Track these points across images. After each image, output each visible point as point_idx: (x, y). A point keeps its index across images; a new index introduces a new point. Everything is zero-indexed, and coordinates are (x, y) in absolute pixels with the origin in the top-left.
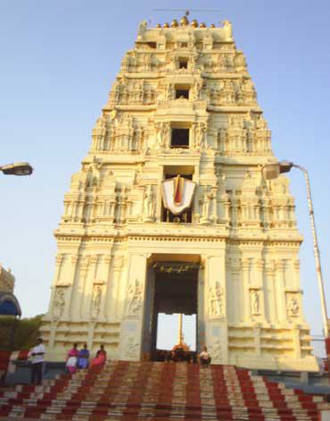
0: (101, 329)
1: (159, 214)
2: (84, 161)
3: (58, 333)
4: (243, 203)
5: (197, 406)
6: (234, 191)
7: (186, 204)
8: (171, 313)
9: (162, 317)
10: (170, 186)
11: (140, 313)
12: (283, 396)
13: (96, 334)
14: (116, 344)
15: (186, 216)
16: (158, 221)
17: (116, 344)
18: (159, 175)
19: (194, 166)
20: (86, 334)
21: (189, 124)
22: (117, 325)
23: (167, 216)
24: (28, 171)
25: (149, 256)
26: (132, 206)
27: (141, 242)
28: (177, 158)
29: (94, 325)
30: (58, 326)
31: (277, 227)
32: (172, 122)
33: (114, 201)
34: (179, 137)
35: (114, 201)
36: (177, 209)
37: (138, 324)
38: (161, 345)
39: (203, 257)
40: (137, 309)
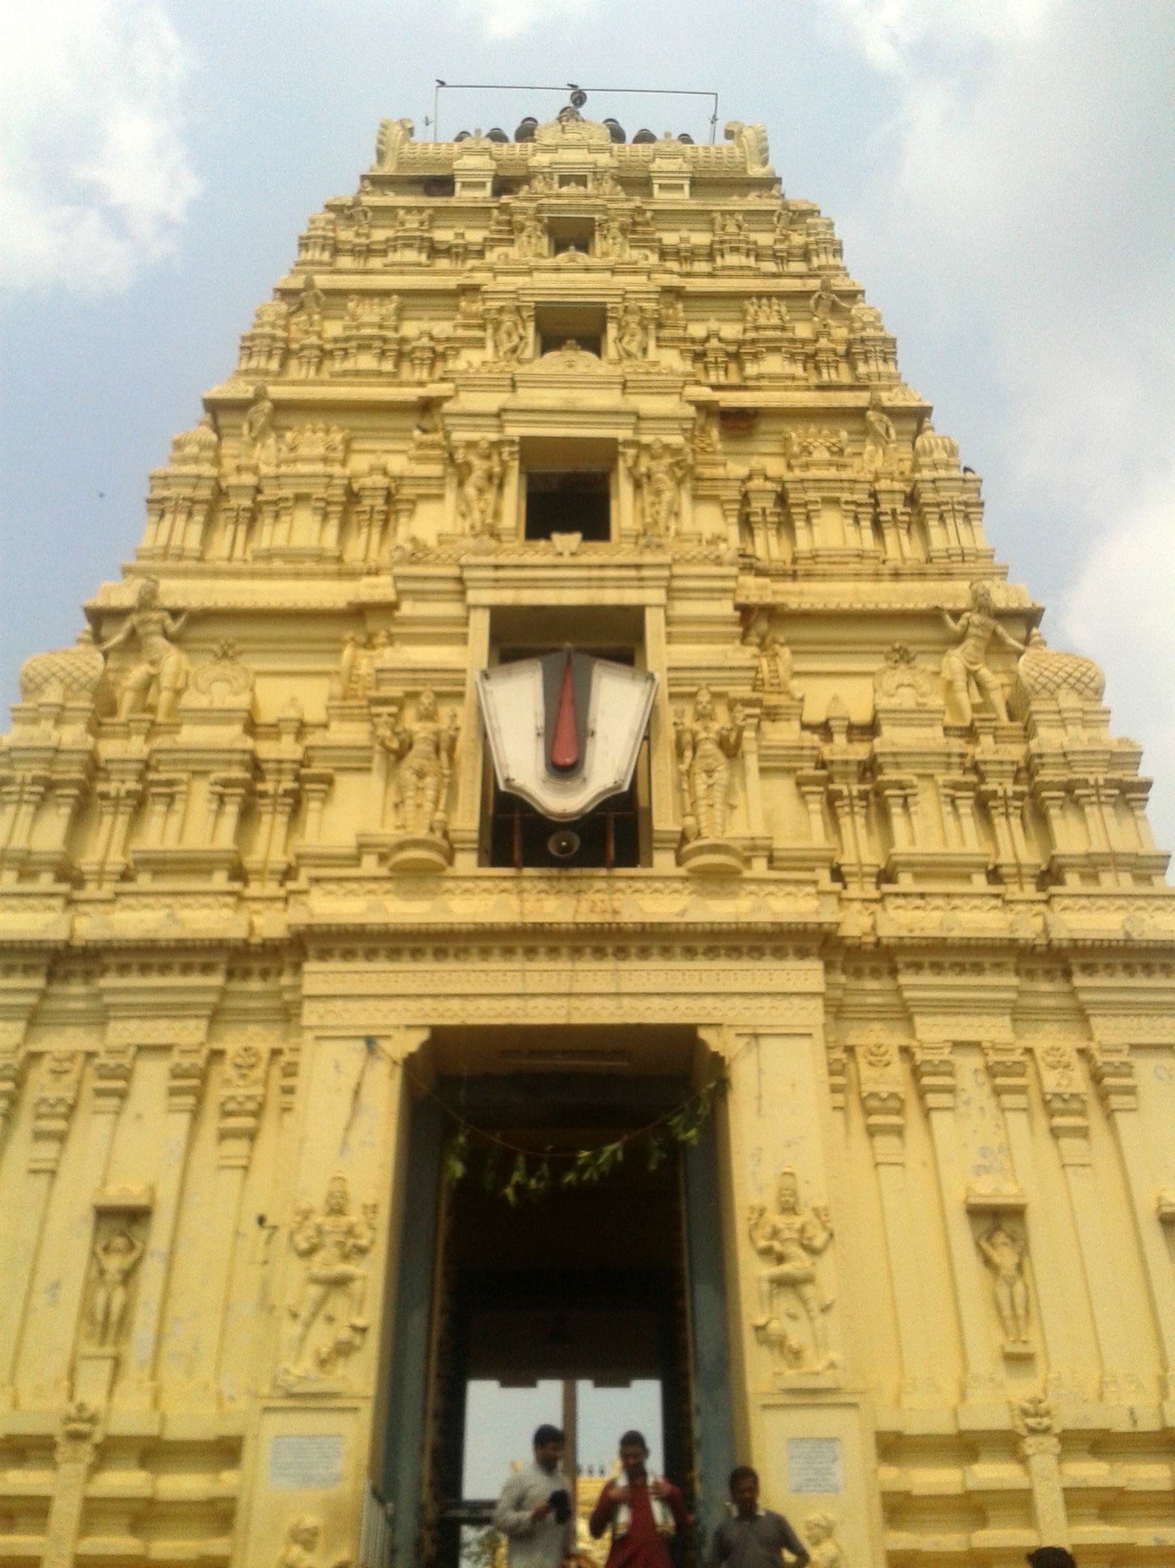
0: (124, 1480)
1: (467, 819)
2: (100, 601)
3: (95, 1512)
4: (890, 775)
5: (756, 171)
8: (530, 1382)
9: (485, 1398)
11: (361, 1376)
13: (95, 1512)
15: (614, 833)
16: (467, 862)
21: (609, 450)
22: (226, 1451)
23: (516, 834)
24: (747, 1483)
25: (413, 1042)
28: (565, 575)
29: (86, 1452)
30: (96, 1468)
31: (1073, 882)
32: (525, 441)
35: (237, 773)
37: (344, 1443)
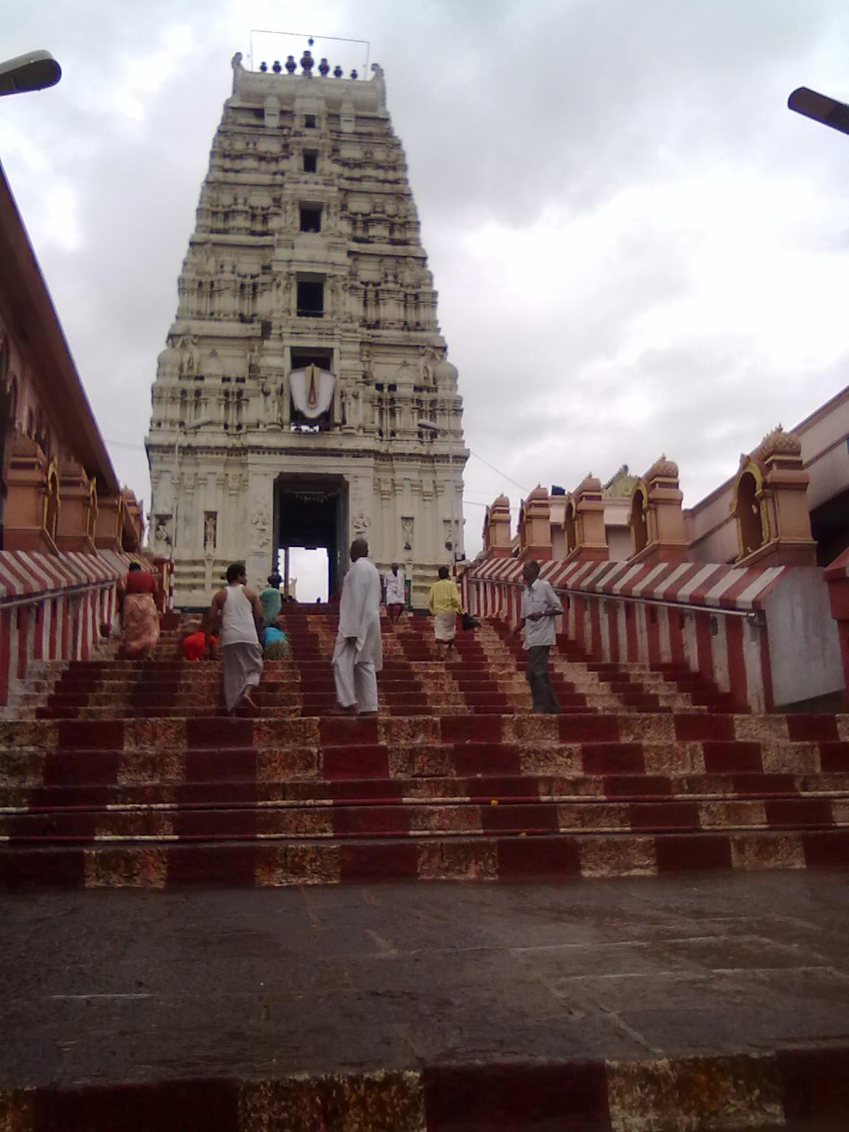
6: (386, 386)
7: (323, 406)
8: (315, 549)
10: (299, 382)
12: (482, 649)
14: (442, 491)
17: (442, 491)
18: (286, 362)
19: (332, 349)
20: (203, 575)
21: (323, 276)
26: (247, 406)
27: (265, 458)
28: (311, 336)
33: (222, 396)
34: (310, 296)
36: (312, 414)
38: (260, 335)
39: (347, 478)
40: (264, 544)
